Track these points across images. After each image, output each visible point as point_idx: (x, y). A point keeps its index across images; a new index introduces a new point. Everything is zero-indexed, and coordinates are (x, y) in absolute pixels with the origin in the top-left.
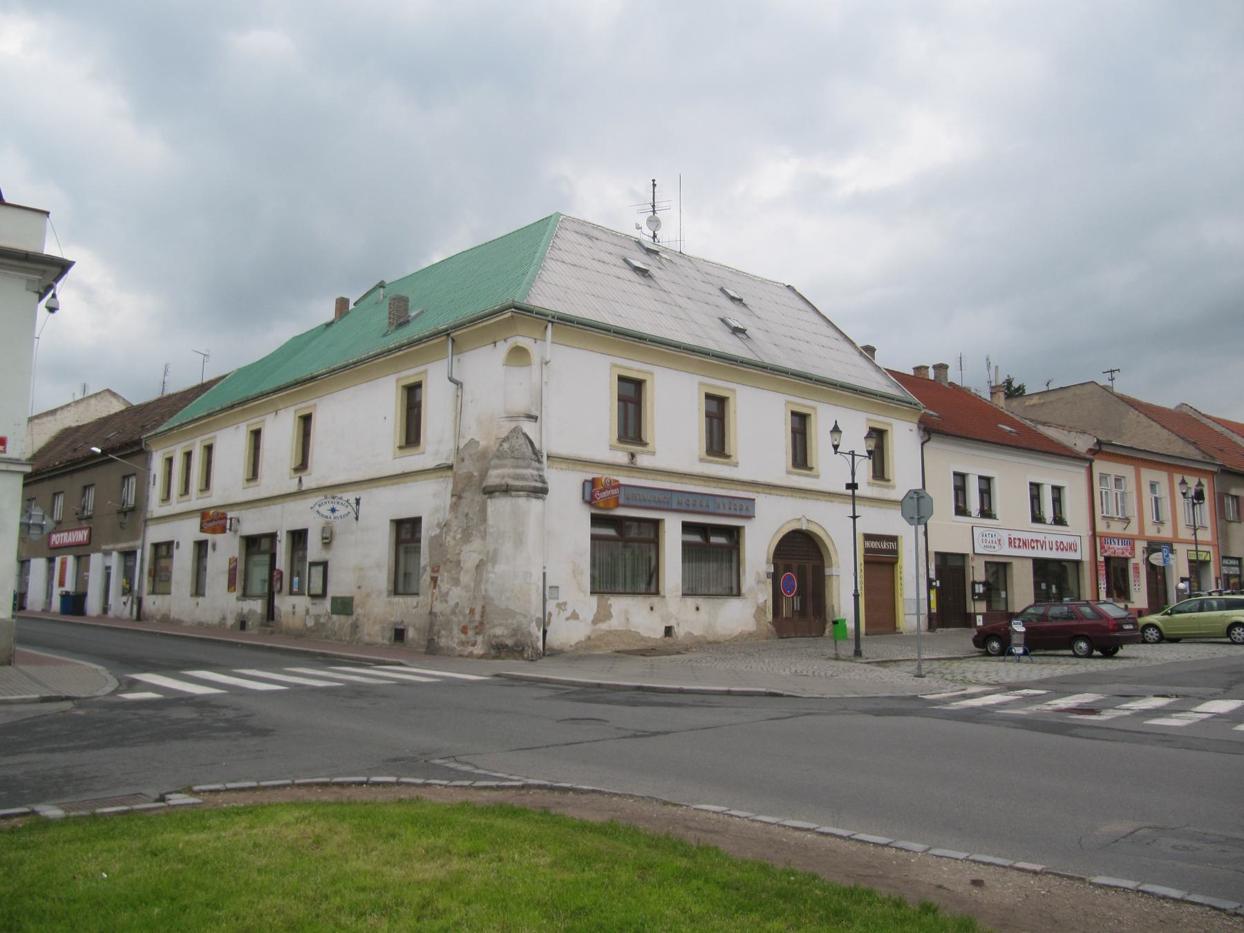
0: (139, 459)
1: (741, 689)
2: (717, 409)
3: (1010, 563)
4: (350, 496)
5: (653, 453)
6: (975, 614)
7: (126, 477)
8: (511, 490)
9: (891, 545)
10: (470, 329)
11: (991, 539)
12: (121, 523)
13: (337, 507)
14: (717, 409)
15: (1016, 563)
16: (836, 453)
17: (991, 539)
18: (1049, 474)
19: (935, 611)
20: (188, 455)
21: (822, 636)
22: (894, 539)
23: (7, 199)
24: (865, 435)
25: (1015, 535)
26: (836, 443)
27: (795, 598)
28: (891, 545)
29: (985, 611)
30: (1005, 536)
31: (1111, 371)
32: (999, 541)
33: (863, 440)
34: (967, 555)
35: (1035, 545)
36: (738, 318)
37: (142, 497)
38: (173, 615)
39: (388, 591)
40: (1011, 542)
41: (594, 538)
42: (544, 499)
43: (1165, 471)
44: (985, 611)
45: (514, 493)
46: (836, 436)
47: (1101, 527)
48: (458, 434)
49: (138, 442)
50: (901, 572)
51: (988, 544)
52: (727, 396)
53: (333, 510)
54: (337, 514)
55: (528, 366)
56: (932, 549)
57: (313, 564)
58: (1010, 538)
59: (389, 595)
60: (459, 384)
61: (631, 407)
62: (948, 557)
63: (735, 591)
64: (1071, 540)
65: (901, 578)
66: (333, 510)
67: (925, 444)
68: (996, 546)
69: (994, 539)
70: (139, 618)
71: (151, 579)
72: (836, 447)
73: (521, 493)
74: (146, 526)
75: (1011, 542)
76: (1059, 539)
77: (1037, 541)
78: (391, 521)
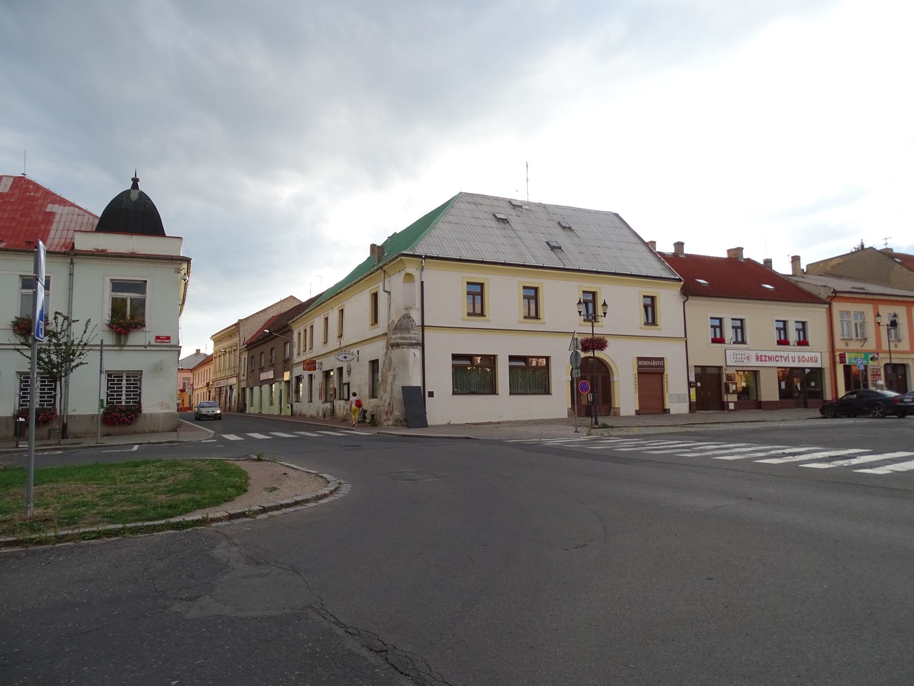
0: (289, 333)
2: (532, 295)
3: (759, 371)
4: (355, 350)
6: (728, 403)
7: (286, 343)
8: (399, 345)
9: (661, 363)
10: (389, 265)
11: (741, 356)
12: (284, 367)
13: (347, 355)
14: (532, 295)
15: (762, 371)
16: (580, 315)
17: (741, 356)
18: (793, 313)
19: (695, 400)
20: (305, 331)
21: (609, 415)
22: (662, 359)
23: (167, 235)
25: (760, 353)
27: (589, 394)
28: (661, 363)
29: (736, 400)
30: (753, 354)
31: (886, 239)
32: (748, 357)
34: (722, 367)
35: (780, 359)
36: (561, 238)
37: (291, 353)
38: (303, 413)
39: (369, 396)
40: (758, 358)
41: (454, 366)
43: (904, 305)
44: (736, 400)
45: (401, 347)
46: (878, 318)
47: (839, 345)
48: (389, 318)
49: (287, 325)
50: (667, 378)
51: (738, 360)
53: (345, 357)
55: (411, 282)
56: (692, 363)
57: (345, 384)
58: (757, 356)
59: (370, 398)
60: (389, 293)
61: (533, 302)
62: (707, 368)
63: (548, 392)
64: (812, 355)
65: (667, 382)
66: (345, 357)
67: (686, 303)
68: (745, 361)
69: (743, 357)
70: (292, 415)
71: (296, 395)
73: (405, 346)
74: (292, 368)
75: (758, 358)
76: (801, 354)
77: (781, 357)
78: (369, 361)
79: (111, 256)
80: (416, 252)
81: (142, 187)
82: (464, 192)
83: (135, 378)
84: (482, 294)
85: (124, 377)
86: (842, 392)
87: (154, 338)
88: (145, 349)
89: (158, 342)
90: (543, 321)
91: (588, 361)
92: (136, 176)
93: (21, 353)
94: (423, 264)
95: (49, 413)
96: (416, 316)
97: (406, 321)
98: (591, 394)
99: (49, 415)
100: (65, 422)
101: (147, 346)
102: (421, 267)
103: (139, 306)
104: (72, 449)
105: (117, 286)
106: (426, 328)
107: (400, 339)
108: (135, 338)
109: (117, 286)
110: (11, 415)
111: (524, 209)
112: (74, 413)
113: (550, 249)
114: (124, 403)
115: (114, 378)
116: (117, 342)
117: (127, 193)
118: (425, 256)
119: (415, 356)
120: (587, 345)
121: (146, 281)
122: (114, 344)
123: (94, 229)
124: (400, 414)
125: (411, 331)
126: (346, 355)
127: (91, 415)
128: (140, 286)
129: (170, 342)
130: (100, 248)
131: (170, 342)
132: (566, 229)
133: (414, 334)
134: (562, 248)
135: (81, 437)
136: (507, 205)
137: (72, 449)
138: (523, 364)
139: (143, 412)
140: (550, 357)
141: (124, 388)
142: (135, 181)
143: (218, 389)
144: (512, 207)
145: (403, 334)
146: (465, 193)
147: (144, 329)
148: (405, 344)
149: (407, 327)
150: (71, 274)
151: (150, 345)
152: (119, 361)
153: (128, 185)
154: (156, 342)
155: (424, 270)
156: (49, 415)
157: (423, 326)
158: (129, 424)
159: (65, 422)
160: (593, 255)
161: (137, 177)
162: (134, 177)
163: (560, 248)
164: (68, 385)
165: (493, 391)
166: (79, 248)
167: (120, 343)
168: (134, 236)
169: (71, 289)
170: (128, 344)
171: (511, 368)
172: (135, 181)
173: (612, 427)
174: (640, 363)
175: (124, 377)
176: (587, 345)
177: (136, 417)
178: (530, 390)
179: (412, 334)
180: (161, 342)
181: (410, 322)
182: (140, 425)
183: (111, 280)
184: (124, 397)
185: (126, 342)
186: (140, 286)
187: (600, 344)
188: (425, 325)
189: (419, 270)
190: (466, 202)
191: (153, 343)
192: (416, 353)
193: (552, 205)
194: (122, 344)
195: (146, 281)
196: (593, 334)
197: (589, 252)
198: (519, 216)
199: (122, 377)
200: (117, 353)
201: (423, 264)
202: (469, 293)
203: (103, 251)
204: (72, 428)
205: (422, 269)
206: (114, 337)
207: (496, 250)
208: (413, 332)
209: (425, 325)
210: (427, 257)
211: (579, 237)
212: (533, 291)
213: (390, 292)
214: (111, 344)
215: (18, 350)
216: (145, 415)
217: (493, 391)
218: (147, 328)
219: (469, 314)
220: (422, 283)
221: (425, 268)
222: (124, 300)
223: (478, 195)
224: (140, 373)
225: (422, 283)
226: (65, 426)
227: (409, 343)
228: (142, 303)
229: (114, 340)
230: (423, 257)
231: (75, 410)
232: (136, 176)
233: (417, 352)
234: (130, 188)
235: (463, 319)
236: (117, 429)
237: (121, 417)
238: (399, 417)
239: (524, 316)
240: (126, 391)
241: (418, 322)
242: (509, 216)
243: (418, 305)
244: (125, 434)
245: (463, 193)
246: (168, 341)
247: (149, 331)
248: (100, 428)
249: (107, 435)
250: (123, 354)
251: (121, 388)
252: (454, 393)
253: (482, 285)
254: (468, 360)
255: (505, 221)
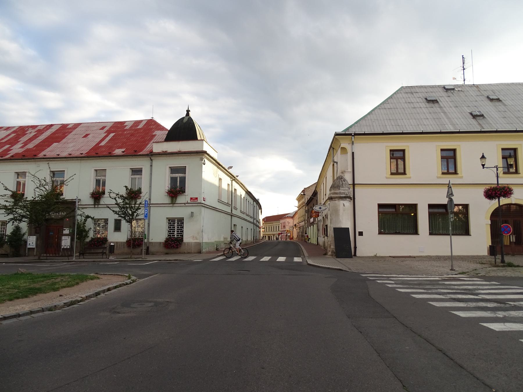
1: (328, 266)
5: (410, 178)
16: (483, 168)
24: (481, 157)
26: (484, 163)
27: (511, 236)
33: (480, 160)
36: (487, 108)
42: (259, 199)
45: (333, 199)
46: (483, 160)
52: (517, 147)
53: (320, 208)
54: (322, 209)
61: (451, 161)
66: (320, 208)
72: (483, 165)
79: (157, 155)
80: (484, 129)
81: (191, 115)
82: (405, 86)
83: (181, 221)
84: (454, 158)
85: (176, 221)
86: (509, 244)
87: (190, 199)
88: (185, 205)
89: (192, 201)
90: (461, 176)
91: (510, 207)
92: (188, 109)
93: (109, 208)
94: (353, 140)
95: (140, 240)
96: (348, 177)
97: (338, 181)
98: (514, 236)
99: (140, 242)
100: (148, 246)
101: (186, 203)
102: (352, 142)
103: (183, 180)
104: (125, 261)
105: (173, 170)
106: (356, 185)
107: (333, 194)
108: (181, 199)
109: (173, 170)
110: (125, 241)
111: (456, 91)
112: (152, 241)
113: (472, 117)
114: (176, 236)
115: (171, 221)
116: (171, 202)
117: (183, 118)
118: (354, 134)
119: (344, 206)
120: (490, 193)
121: (186, 167)
122: (170, 203)
123: (163, 140)
124: (334, 247)
125: (341, 188)
126: (321, 207)
127: (159, 242)
128: (183, 170)
129: (197, 201)
130: (164, 150)
131: (197, 201)
132: (494, 101)
133: (344, 190)
134: (484, 115)
135: (155, 254)
136: (441, 90)
137: (125, 261)
138: (394, 210)
139: (184, 241)
140: (469, 204)
141: (176, 228)
142: (188, 111)
143: (299, 228)
144: (445, 90)
145: (335, 190)
146: (406, 87)
147: (184, 194)
148: (336, 198)
149: (338, 186)
150: (151, 166)
151: (188, 203)
152: (176, 212)
153: (184, 114)
154: (191, 201)
155: (354, 144)
156: (140, 242)
157: (354, 185)
158: (177, 248)
159: (148, 246)
160: (517, 118)
161: (189, 109)
162: (187, 109)
163: (482, 115)
164: (149, 226)
165: (415, 231)
166: (154, 152)
167: (173, 202)
168: (180, 142)
169: (151, 174)
170: (176, 203)
171: (430, 214)
172: (188, 111)
173: (518, 266)
174: (432, 210)
175: (176, 221)
176: (490, 193)
177: (181, 244)
178: (388, 230)
179: (341, 190)
180: (193, 201)
181: (341, 182)
182: (182, 249)
183: (170, 167)
184: (176, 233)
185: (175, 202)
186: (183, 170)
187: (503, 192)
188: (355, 183)
189: (351, 145)
190: (404, 93)
191: (189, 202)
192: (345, 204)
193: (485, 85)
194: (174, 202)
195: (186, 167)
196: (498, 184)
197: (512, 115)
198: (449, 96)
199: (175, 221)
200: (171, 208)
201: (353, 140)
202: (442, 158)
203: (166, 152)
204: (151, 249)
205: (353, 143)
206: (170, 199)
207: (419, 124)
208: (343, 188)
209: (355, 183)
210: (356, 134)
211: (506, 105)
212: (402, 152)
213: (337, 162)
214: (168, 203)
215: (108, 207)
216: (185, 243)
217: (415, 231)
218: (186, 193)
219: (392, 174)
220: (353, 153)
221: (354, 142)
222: (176, 178)
223: (417, 86)
224: (107, 220)
225: (353, 153)
226: (148, 248)
227: (339, 197)
228: (184, 178)
229: (170, 201)
230: (353, 134)
231: (152, 239)
232: (188, 109)
233: (348, 204)
234: (185, 116)
235: (387, 178)
236: (171, 251)
237: (172, 244)
238: (333, 249)
239: (503, 172)
240: (177, 229)
241: (350, 182)
242: (440, 98)
243: (350, 169)
244: (175, 253)
245: (403, 87)
246: (197, 200)
247: (187, 195)
248: (162, 249)
249: (167, 254)
250: (174, 208)
251: (175, 227)
252: (380, 233)
253: (404, 151)
254: (394, 209)
255: (435, 101)
